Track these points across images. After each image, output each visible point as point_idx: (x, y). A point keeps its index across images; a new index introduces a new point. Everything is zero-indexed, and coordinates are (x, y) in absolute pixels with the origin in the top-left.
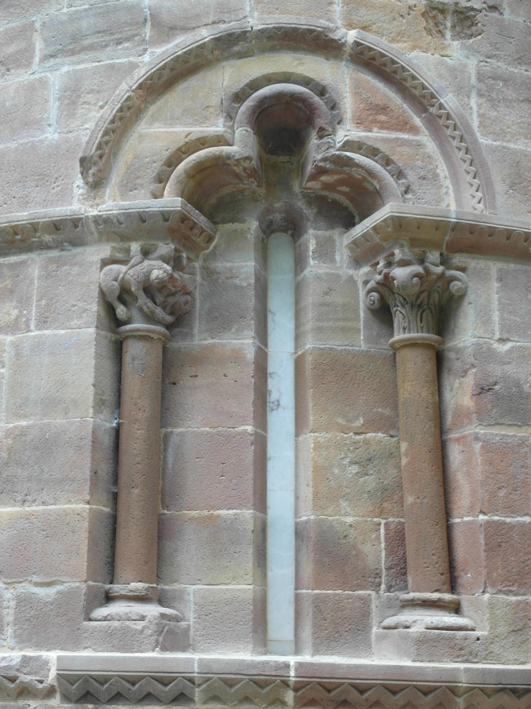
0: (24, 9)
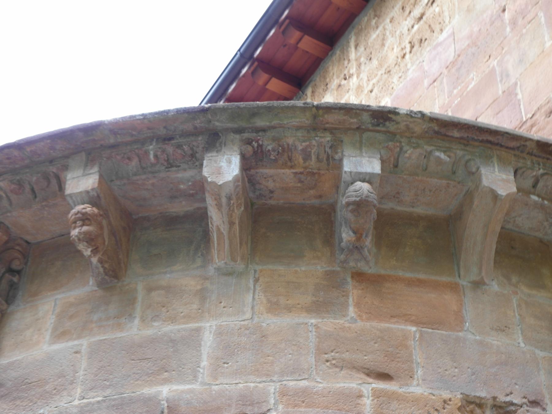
0: (31, 401)
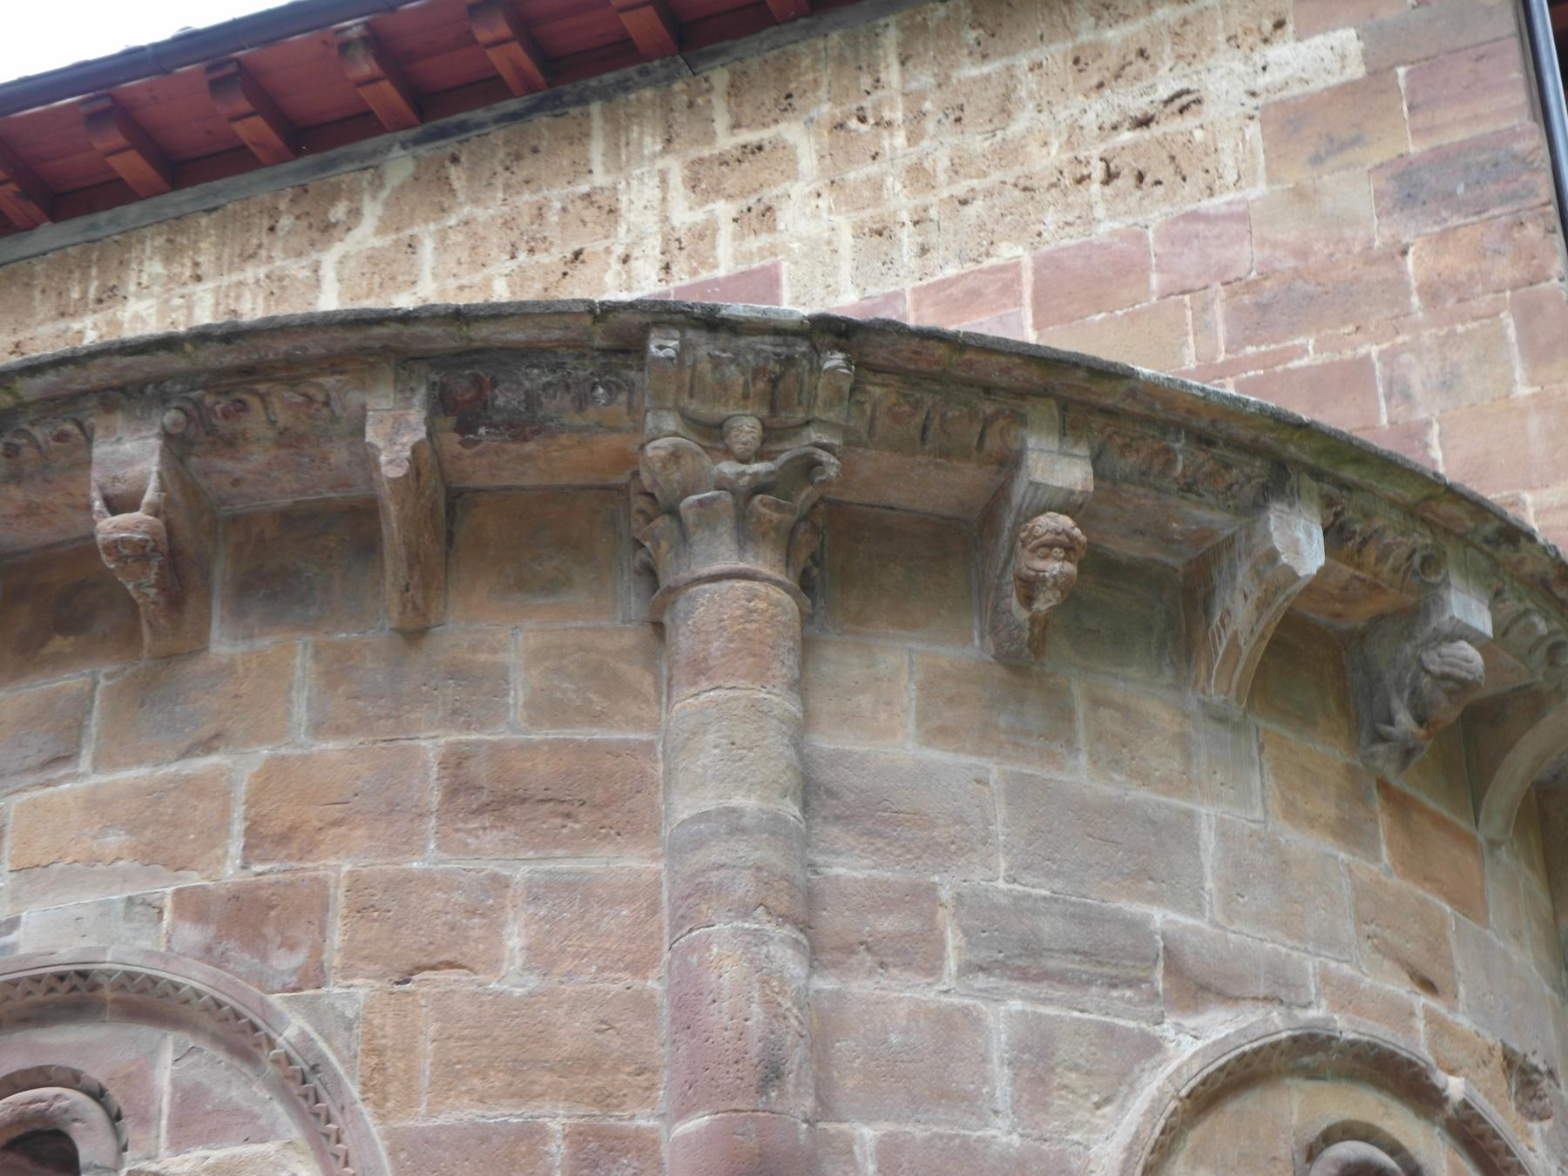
0: (909, 851)
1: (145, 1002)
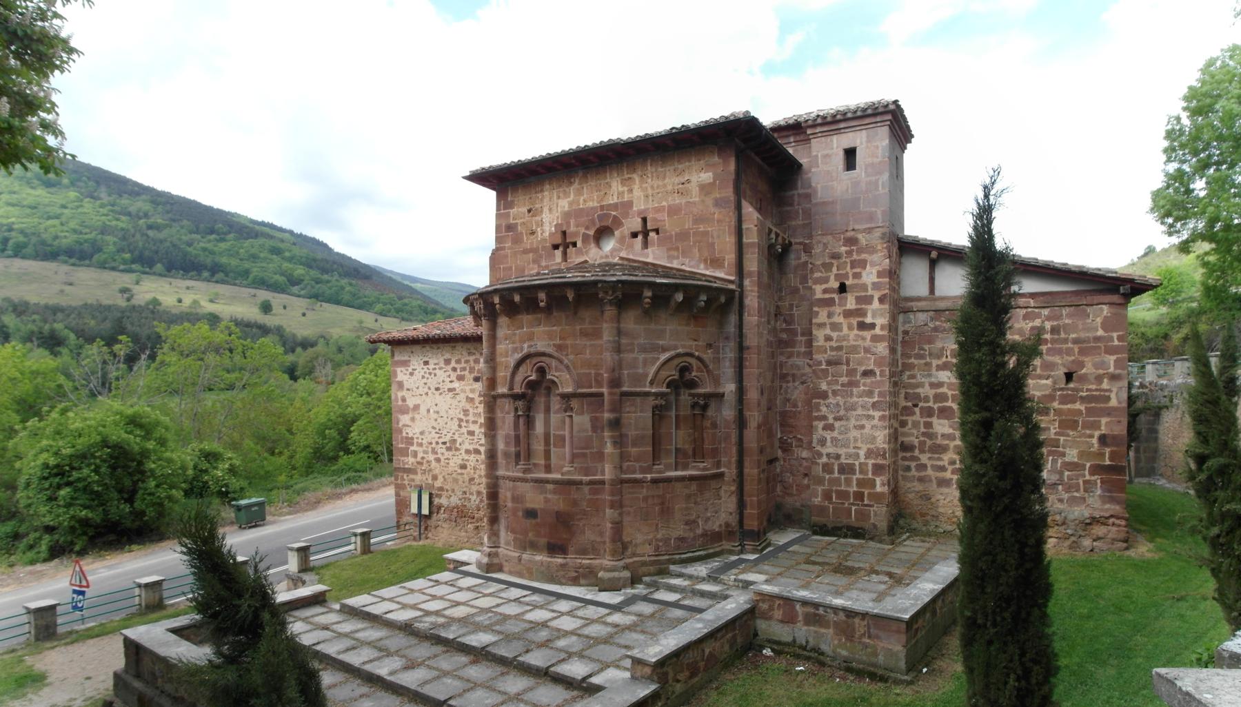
1: (550, 356)
